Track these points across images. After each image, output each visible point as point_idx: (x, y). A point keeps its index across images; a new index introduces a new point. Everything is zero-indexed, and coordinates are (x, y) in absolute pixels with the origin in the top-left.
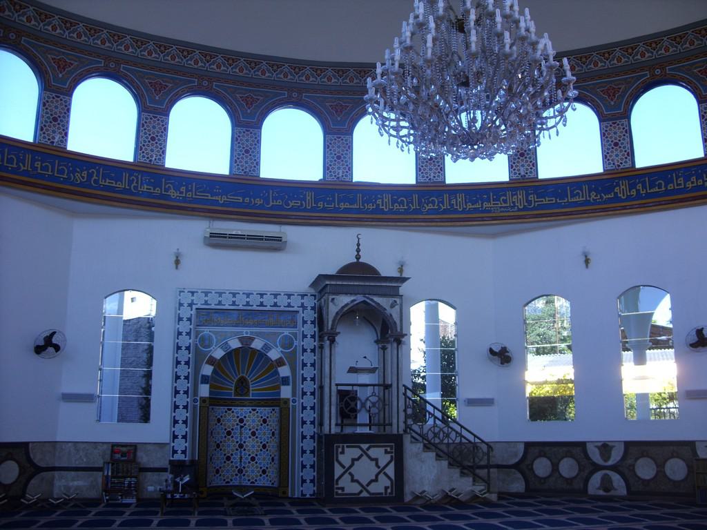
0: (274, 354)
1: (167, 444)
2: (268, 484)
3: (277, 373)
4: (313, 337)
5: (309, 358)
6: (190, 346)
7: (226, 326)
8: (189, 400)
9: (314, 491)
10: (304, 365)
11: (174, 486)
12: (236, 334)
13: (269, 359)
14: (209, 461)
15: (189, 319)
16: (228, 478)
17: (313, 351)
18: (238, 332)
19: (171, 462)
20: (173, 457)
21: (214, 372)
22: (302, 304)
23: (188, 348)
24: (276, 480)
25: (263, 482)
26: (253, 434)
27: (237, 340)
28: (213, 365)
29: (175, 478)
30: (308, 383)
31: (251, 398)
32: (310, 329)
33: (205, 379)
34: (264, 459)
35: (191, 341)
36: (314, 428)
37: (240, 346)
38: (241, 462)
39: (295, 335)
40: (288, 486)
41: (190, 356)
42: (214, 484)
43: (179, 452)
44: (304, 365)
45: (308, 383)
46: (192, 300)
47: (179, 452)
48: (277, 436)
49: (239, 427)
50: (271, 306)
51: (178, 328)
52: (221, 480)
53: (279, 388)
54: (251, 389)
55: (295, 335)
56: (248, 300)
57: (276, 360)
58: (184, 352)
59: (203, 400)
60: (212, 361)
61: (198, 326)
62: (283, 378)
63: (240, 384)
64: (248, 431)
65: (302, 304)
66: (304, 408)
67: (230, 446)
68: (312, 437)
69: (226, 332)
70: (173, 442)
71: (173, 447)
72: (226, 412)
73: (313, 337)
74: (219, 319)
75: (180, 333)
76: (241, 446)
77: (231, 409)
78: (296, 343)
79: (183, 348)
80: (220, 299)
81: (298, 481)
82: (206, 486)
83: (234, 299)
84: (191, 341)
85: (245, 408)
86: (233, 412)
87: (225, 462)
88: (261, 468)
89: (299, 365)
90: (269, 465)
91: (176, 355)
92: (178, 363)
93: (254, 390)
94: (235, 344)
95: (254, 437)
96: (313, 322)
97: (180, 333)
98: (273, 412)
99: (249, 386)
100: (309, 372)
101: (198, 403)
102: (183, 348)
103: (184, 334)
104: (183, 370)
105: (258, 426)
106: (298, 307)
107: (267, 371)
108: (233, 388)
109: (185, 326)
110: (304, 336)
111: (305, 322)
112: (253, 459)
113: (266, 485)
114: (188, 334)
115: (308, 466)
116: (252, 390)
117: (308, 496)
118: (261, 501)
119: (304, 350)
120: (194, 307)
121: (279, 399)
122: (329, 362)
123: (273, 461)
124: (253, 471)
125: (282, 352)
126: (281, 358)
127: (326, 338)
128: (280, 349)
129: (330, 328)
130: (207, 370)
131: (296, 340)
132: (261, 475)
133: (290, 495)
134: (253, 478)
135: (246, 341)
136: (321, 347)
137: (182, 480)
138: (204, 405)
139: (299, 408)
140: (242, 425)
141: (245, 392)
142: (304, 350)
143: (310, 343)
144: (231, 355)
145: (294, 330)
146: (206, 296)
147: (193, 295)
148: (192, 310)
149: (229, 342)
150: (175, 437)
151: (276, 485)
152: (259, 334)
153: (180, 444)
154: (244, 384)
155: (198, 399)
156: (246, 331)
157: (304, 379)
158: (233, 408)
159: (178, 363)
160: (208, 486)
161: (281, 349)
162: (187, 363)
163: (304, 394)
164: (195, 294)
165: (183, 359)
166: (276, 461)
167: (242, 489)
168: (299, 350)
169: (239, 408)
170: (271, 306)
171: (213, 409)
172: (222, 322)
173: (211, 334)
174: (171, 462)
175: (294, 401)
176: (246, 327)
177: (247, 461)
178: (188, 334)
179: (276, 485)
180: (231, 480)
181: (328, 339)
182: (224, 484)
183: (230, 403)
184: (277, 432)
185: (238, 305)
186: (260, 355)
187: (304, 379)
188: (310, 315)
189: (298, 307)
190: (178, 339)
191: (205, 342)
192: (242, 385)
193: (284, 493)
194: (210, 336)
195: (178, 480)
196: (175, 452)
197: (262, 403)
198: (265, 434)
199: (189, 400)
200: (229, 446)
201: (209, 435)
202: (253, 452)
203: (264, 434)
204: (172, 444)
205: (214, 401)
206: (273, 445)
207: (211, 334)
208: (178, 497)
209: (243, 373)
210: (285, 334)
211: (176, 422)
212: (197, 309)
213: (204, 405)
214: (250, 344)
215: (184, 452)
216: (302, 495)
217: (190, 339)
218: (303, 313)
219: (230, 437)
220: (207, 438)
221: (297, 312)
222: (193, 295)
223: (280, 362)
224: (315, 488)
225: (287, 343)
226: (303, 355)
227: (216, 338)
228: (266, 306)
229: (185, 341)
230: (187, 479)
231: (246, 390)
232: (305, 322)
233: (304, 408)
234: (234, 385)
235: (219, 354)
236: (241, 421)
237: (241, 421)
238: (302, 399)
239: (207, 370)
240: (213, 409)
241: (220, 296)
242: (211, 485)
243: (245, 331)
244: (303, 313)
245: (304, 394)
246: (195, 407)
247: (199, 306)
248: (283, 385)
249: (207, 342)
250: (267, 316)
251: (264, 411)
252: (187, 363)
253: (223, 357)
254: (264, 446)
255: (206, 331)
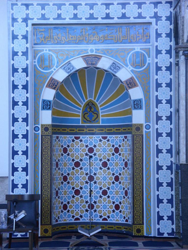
0: (124, 74)
1: (7, 177)
2: (122, 221)
3: (127, 96)
4: (169, 52)
5: (164, 77)
6: (27, 68)
7: (68, 43)
8: (28, 128)
9: (173, 229)
10: (158, 85)
11: (8, 224)
12: (80, 52)
13: (118, 80)
14: (54, 196)
15: (25, 37)
16: (77, 214)
17: (169, 69)
18: (82, 51)
19: (8, 197)
20: (13, 192)
21: (57, 96)
22: (156, 13)
23: (25, 70)
24: (130, 216)
25: (117, 218)
26: (105, 165)
27: (81, 59)
28: (54, 88)
29: (9, 214)
30: (164, 89)
31: (101, 124)
32: (165, 43)
33: (47, 105)
34: (117, 193)
35: (28, 62)
36: (172, 157)
37: (85, 66)
38: (90, 196)
39: (148, 51)
40: (143, 224)
41: (28, 79)
42: (61, 221)
43: (20, 186)
44: (158, 85)
45: (164, 89)
46: (27, 15)
47: (20, 186)
48: (130, 166)
49: (88, 157)
50: (118, 18)
51: (13, 48)
52: (69, 216)
53: (131, 113)
54: (101, 114)
55: (148, 51)
56: (91, 12)
57: (126, 81)
58: (20, 75)
59: (46, 128)
60: (53, 84)
61: (35, 44)
62: (134, 101)
63: (89, 110)
64: (98, 161)
65: (156, 13)
66: (159, 135)
67: (79, 178)
68: (169, 168)
69: (68, 50)
70: (13, 175)
71: (13, 181)
72: (73, 141)
73: (169, 52)
74: (60, 36)
75: (15, 54)
76: (91, 178)
77: (79, 138)
78: (149, 60)
79: (20, 70)
80: (59, 12)
81: (154, 218)
82: (51, 224)
83: (75, 12)
84: (28, 62)
85: (94, 136)
86: (81, 141)
87: (73, 197)
88: (114, 203)
89: (153, 85)
90: (123, 199)
91: (12, 79)
92: (15, 87)
93: (104, 115)
94: (79, 64)
95: (106, 169)
96: (169, 35)
97: (15, 54)
98: (126, 140)
99: (98, 112)
100: (164, 94)
101: (40, 131)
102: (20, 70)
103: (20, 54)
104: (21, 95)
105: (109, 155)
106: (151, 17)
107: (118, 93)
108: (81, 114)
109: (20, 45)
110: (158, 52)
111: (158, 35)
112: (105, 193)
113: (120, 222)
114: (25, 54)
115: (165, 201)
116: (102, 116)
117: (166, 235)
118: (111, 240)
119: (158, 69)
120: (30, 22)
121: (131, 126)
122: (184, 81)
123: (126, 196)
124: (105, 207)
125: (132, 71)
126: (132, 78)
127: (181, 53)
128: (130, 68)
129: (185, 41)
130: (49, 94)
131: (149, 57)
132: (114, 211)
133: (145, 235)
134: (105, 214)
135: (91, 59)
136: (177, 64)
137: (16, 216)
138: (46, 133)
139: (153, 135)
140: (92, 154)
141: (94, 118)
142: (158, 69)
143: (165, 60)
144: (75, 76)
145: (144, 46)
146: (43, 8)
147: (27, 9)
148: (27, 26)
149: (72, 62)
150: (14, 170)
151: (130, 222)
152: (107, 52)
153: (20, 178)
154: (93, 110)
155: (40, 127)
156: (91, 49)
157: (159, 102)
158: (81, 136)
159: (15, 87)
160: (54, 222)
161: (132, 68)
162: (25, 87)
163: (159, 118)
164: (30, 7)
165: (20, 83)
166: (130, 195)
167: (91, 226)
168: (153, 69)
169: (88, 136)
170: (118, 18)
171: (57, 138)
172: (63, 38)
173: (51, 53)
174: (8, 197)
175: (148, 127)
176: (91, 44)
177: (98, 195)
178: (25, 54)
179: (130, 222)
180: (81, 216)
181: (183, 54)
182: (73, 221)
183: (76, 131)
184: (130, 163)
185: (81, 19)
186: (108, 76)
187: (159, 102)
188: (165, 27)
189: (151, 17)
190: (13, 60)
191: (44, 62)
192: (91, 110)
193: (139, 231)
194: (50, 56)
195: (12, 217)
196: (15, 186)
197: (114, 130)
198: (117, 165)
199: (28, 128)
200: (77, 179)
201: (54, 167)
202: (105, 185)
203: (117, 164)
204: (12, 178)
205: (58, 128)
206: (126, 177)
207: (51, 53)
208: (19, 236)
209: (91, 96)
210: (136, 50)
211: (15, 153)
212: (33, 25)
213: (46, 133)
214: (96, 64)
215: (25, 186)
216: (159, 233)
217: (27, 59)
218: (157, 25)
219: (78, 168)
220: (51, 169)
221: (150, 23)
222: (27, 9)
223: (137, 104)
224: (174, 226)
225: (139, 61)
226: (157, 74)
227: (57, 57)
228: (113, 18)
229: (21, 62)
230: (22, 215)
231: (95, 116)
232: (158, 35)
233: (159, 135)
234: (81, 111)
235: (61, 76)
236: (91, 150)
237: (91, 150)
238: (157, 124)
239: (49, 94)
240: (57, 138)
241: (59, 8)
242: (59, 222)
243: (90, 49)
244: (157, 25)
245: (159, 118)
246: (36, 136)
247: (36, 21)
248: (135, 108)
249: (47, 63)
250: (114, 31)
251: (116, 139)
252: (25, 87)
253: (66, 80)
254: (117, 179)
255: (46, 50)
